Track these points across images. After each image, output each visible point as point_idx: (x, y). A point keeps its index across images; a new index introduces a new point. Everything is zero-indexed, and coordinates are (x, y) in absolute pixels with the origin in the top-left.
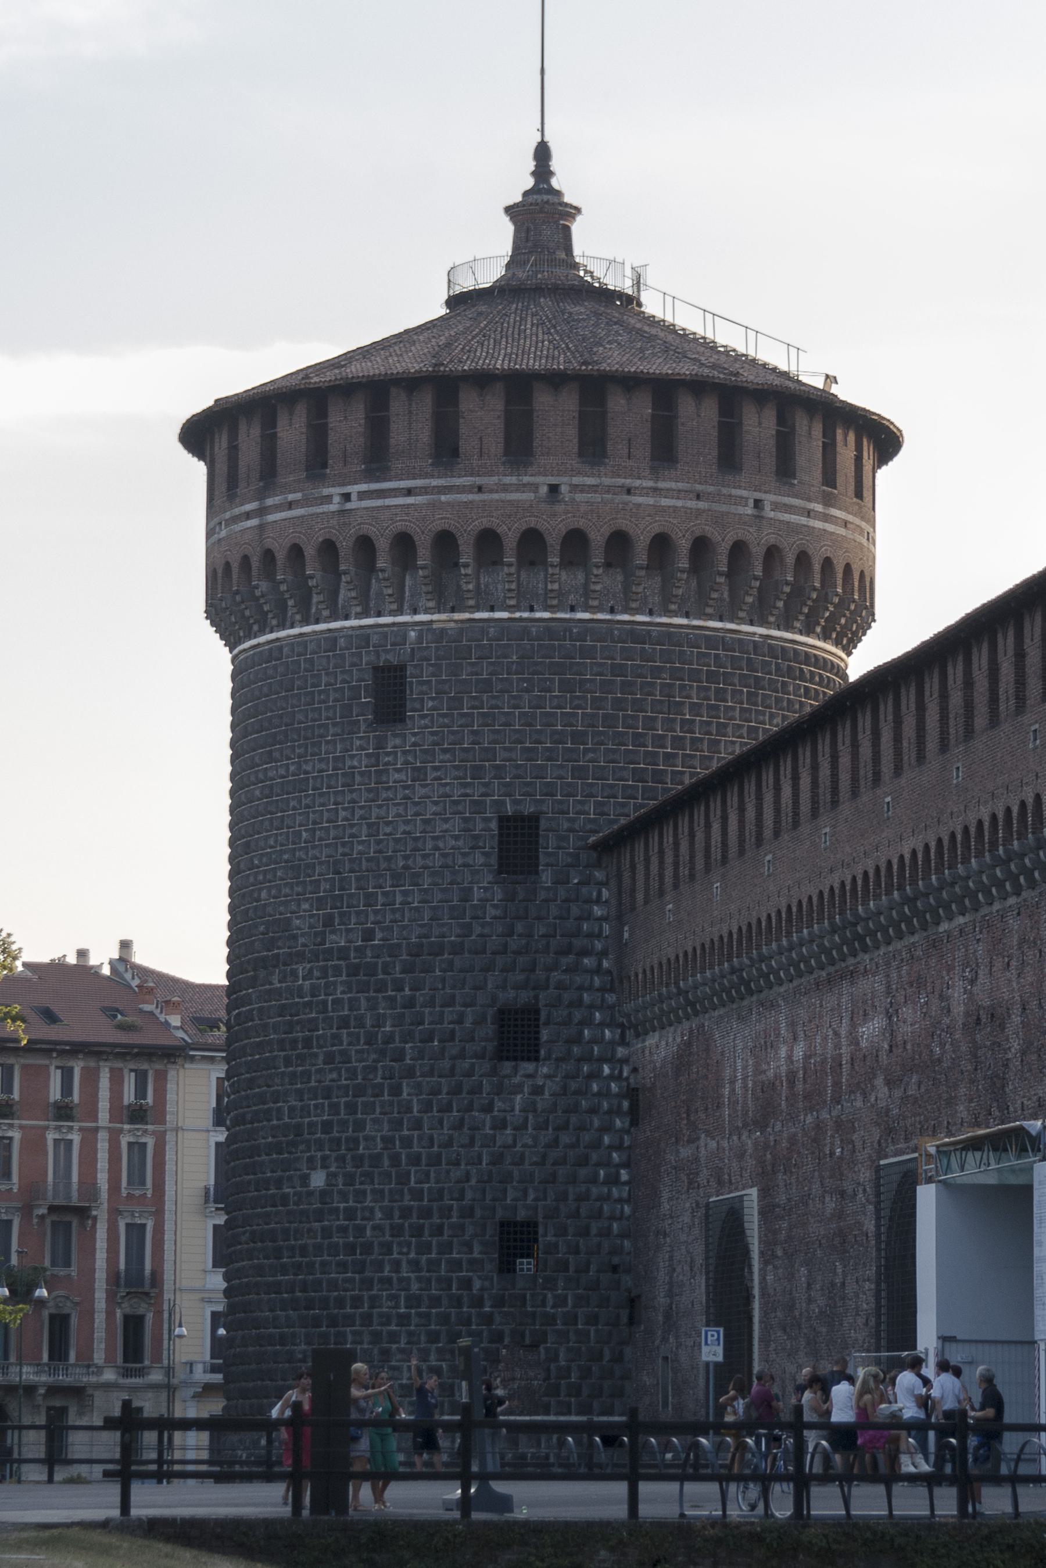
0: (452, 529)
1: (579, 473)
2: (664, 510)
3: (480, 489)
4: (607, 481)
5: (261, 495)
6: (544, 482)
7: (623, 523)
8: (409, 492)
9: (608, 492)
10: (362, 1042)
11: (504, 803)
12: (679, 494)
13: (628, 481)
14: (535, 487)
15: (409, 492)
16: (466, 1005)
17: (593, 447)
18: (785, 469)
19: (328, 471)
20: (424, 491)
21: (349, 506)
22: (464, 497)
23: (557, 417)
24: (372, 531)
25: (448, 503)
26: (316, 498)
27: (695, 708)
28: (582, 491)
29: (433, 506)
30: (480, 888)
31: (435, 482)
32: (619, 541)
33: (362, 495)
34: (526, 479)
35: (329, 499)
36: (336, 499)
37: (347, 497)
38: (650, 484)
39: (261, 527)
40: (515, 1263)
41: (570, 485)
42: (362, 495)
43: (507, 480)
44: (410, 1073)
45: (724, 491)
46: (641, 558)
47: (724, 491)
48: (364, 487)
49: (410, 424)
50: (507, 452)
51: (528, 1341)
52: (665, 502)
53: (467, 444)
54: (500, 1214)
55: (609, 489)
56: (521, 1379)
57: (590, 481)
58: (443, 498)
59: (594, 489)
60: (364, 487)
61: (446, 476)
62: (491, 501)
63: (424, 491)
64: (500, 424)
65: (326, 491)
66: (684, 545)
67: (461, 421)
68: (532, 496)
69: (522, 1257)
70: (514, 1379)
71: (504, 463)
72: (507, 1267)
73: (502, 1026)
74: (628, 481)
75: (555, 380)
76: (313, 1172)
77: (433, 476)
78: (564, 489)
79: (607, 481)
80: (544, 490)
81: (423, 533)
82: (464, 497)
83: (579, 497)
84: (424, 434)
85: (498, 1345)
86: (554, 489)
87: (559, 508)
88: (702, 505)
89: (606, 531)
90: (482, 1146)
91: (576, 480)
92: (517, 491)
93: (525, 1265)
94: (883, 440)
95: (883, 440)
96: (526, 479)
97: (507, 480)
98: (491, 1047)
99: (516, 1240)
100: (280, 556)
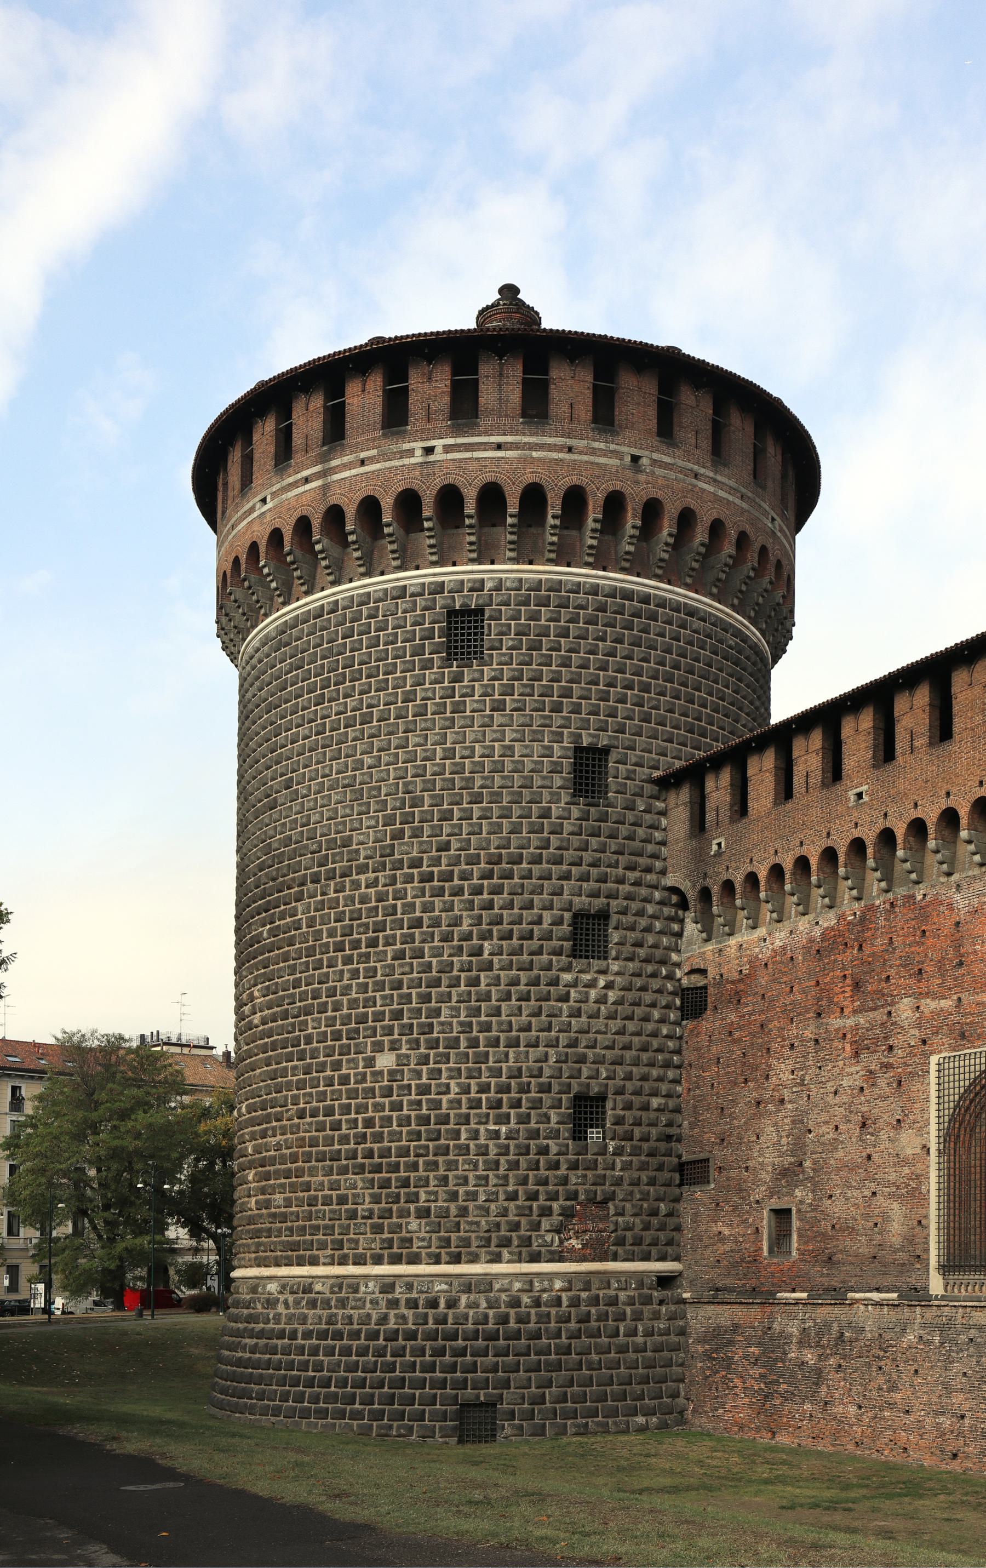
0: (543, 483)
4: (680, 463)
5: (324, 458)
6: (628, 450)
7: (692, 503)
8: (499, 447)
9: (681, 472)
10: (436, 940)
11: (580, 736)
13: (696, 467)
14: (618, 455)
15: (499, 447)
16: (544, 909)
19: (409, 428)
21: (431, 458)
22: (555, 455)
24: (459, 481)
25: (539, 459)
26: (394, 453)
28: (660, 467)
29: (524, 460)
30: (558, 807)
31: (526, 439)
33: (447, 449)
34: (613, 447)
35: (411, 452)
36: (418, 452)
37: (429, 451)
38: (711, 474)
39: (325, 488)
40: (586, 1132)
41: (651, 459)
42: (447, 449)
43: (596, 445)
44: (489, 967)
45: (757, 500)
47: (757, 500)
48: (450, 441)
49: (500, 385)
50: (595, 420)
51: (599, 1199)
52: (721, 493)
54: (575, 1088)
56: (593, 1231)
58: (534, 454)
59: (666, 466)
60: (450, 441)
61: (536, 434)
62: (581, 462)
64: (589, 394)
65: (406, 446)
67: (553, 387)
68: (618, 462)
69: (591, 1127)
70: (585, 1231)
71: (593, 430)
72: (578, 1135)
73: (575, 929)
74: (696, 467)
76: (377, 1055)
77: (524, 434)
78: (645, 461)
81: (514, 484)
82: (555, 455)
83: (658, 471)
84: (515, 395)
85: (573, 1202)
87: (642, 477)
90: (559, 1031)
91: (655, 456)
92: (605, 456)
93: (594, 1134)
96: (613, 447)
97: (596, 445)
98: (567, 945)
99: (586, 1110)
100: (350, 512)
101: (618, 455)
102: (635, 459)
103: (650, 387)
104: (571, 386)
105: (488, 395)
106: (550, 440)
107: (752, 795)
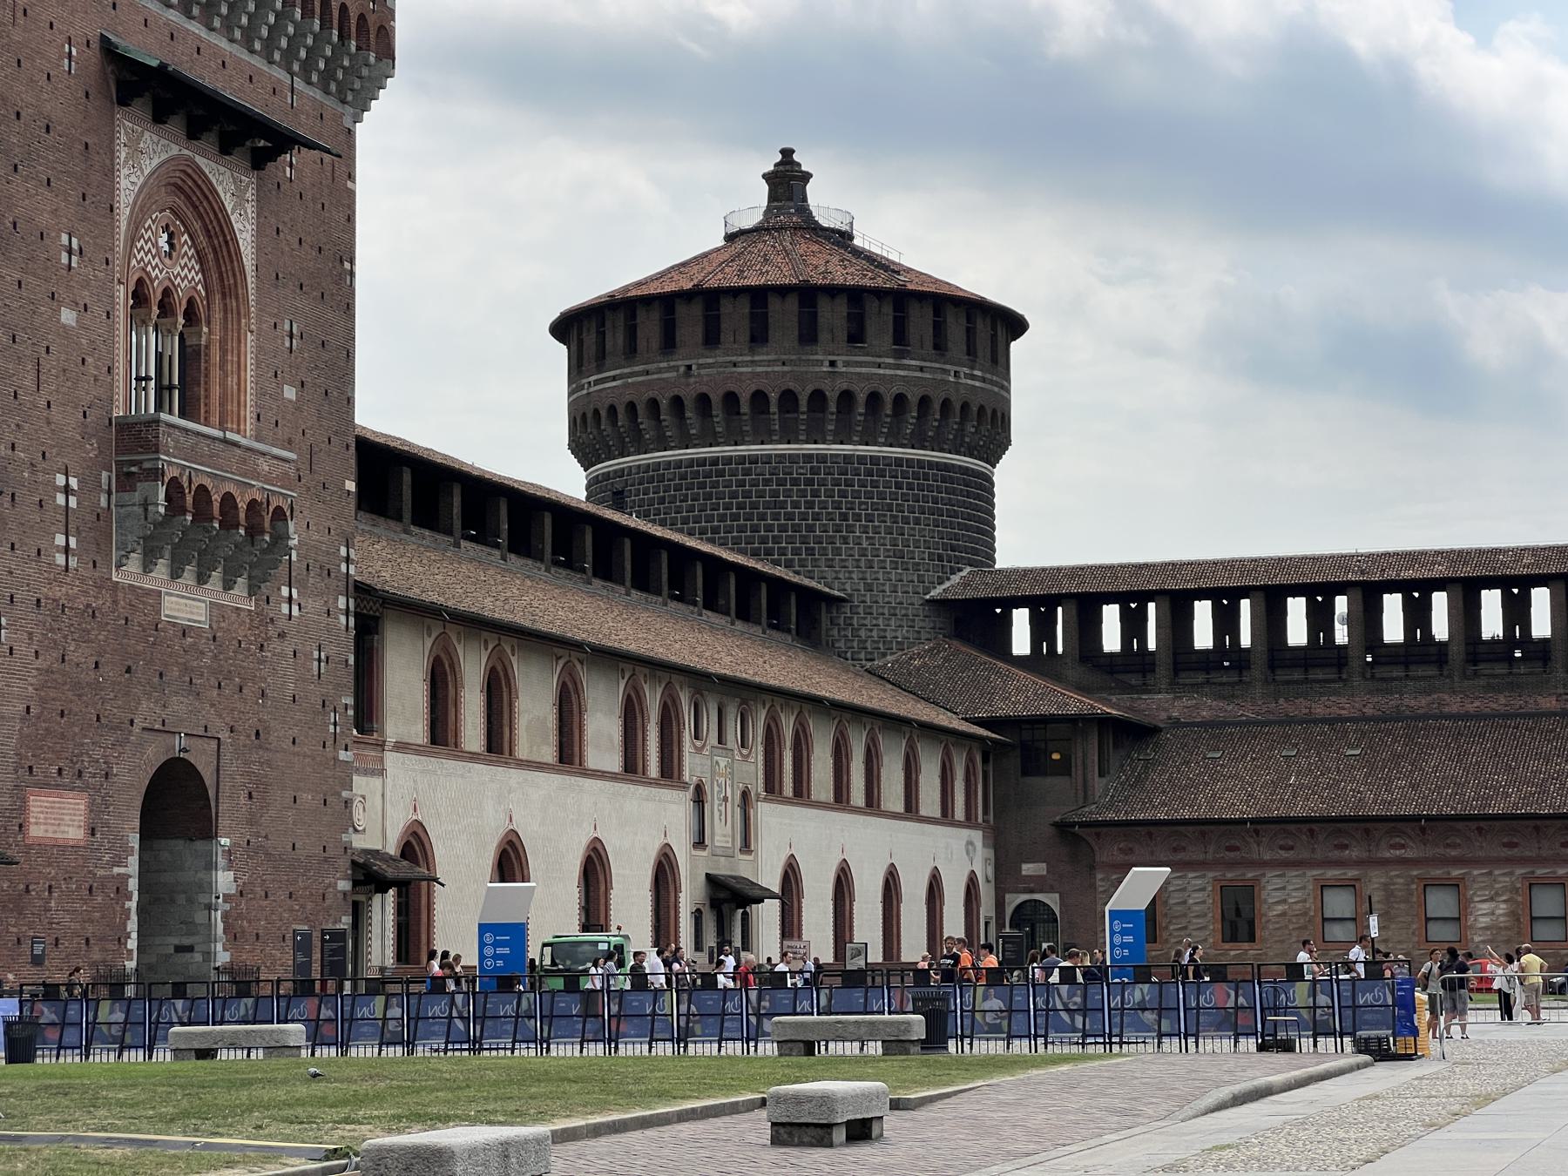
1: (703, 356)
2: (758, 374)
3: (648, 373)
7: (732, 387)
8: (614, 378)
12: (769, 363)
14: (676, 368)
15: (614, 378)
17: (712, 338)
18: (940, 346)
20: (620, 377)
23: (784, 315)
27: (796, 505)
31: (626, 370)
32: (731, 399)
42: (847, 364)
46: (745, 408)
52: (759, 369)
53: (641, 344)
55: (722, 365)
57: (710, 361)
59: (710, 366)
63: (620, 377)
65: (948, 367)
66: (861, 397)
75: (782, 291)
79: (720, 359)
80: (682, 369)
83: (703, 372)
86: (689, 367)
87: (692, 380)
88: (786, 368)
89: (721, 392)
91: (701, 361)
94: (1014, 325)
95: (1014, 325)
101: (676, 368)
102: (689, 367)
103: (929, 312)
104: (879, 321)
105: (871, 328)
106: (636, 369)
107: (542, 626)
